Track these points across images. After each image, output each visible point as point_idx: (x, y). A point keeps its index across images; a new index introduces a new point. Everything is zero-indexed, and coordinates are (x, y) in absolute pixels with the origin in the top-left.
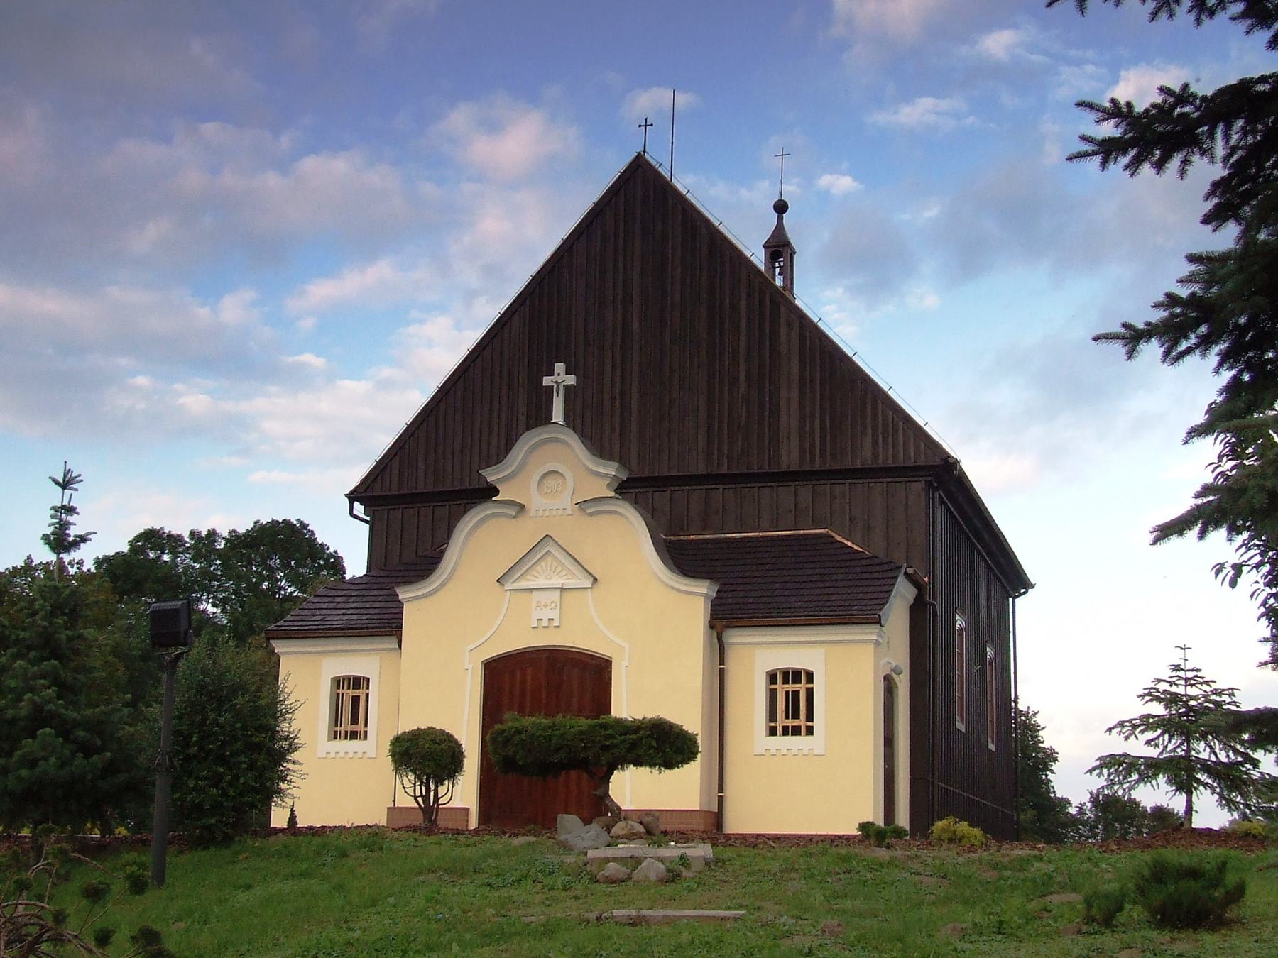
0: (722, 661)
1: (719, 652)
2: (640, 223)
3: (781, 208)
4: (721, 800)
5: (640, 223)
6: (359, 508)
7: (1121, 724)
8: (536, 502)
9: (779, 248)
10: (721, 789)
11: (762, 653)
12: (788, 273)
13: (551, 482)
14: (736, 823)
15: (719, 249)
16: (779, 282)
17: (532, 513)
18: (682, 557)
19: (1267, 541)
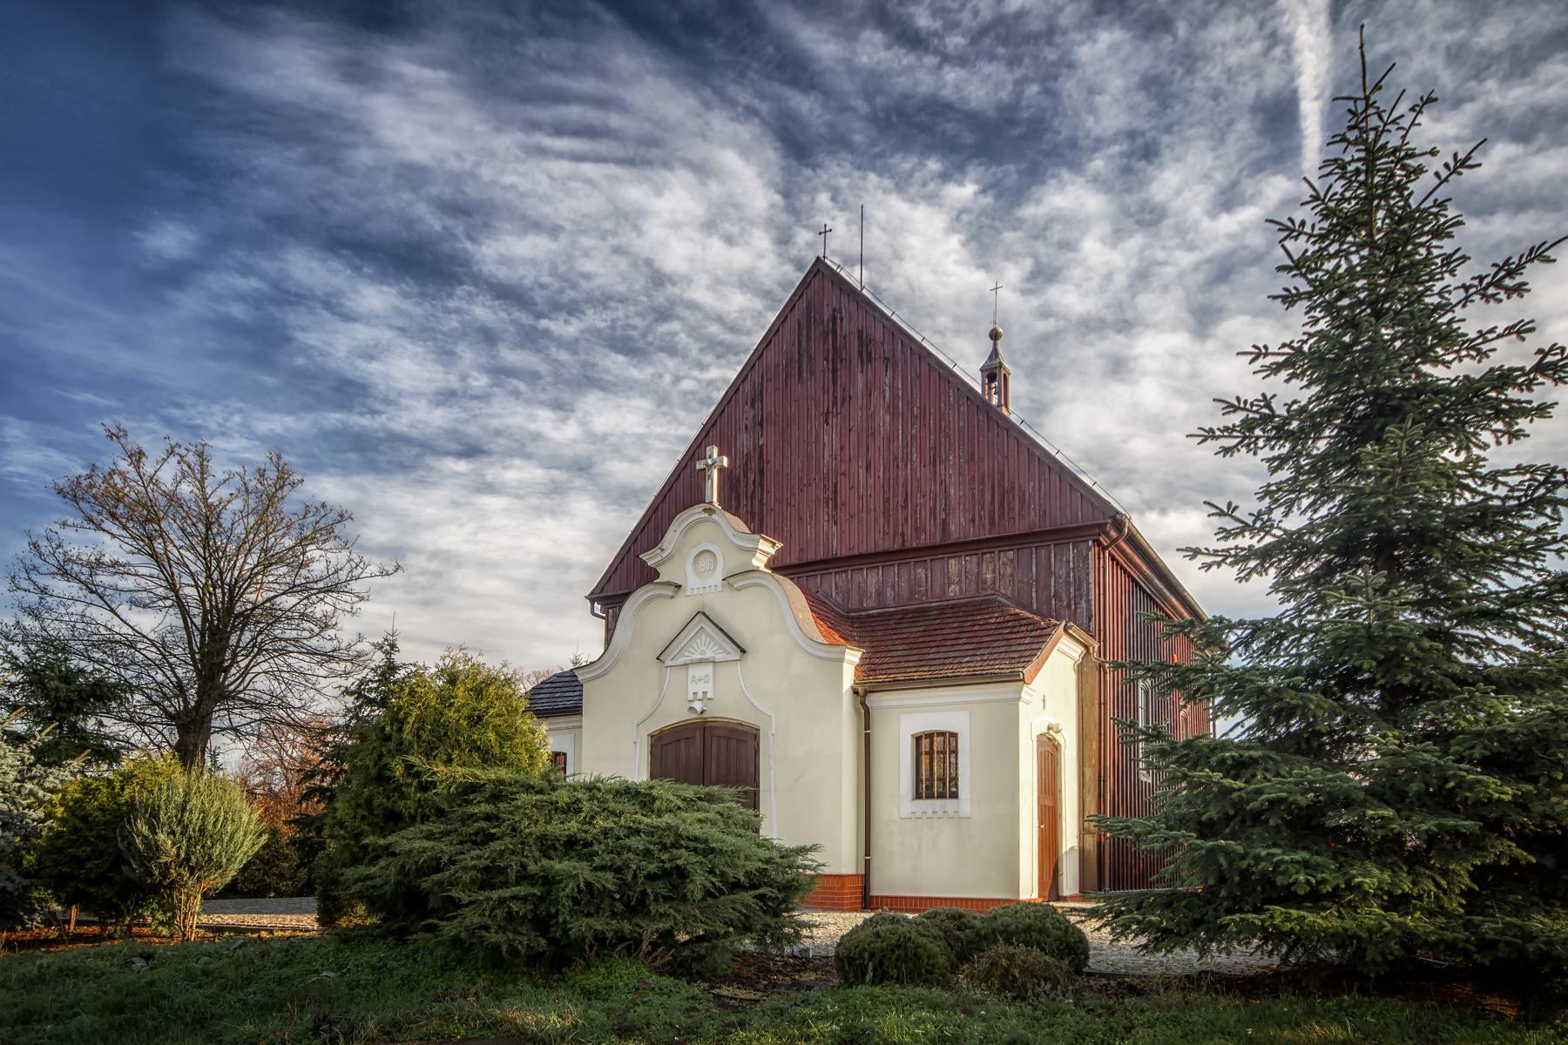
0: (867, 727)
1: (866, 718)
2: (830, 333)
3: (995, 336)
4: (868, 863)
5: (830, 333)
6: (597, 607)
7: (1188, 549)
8: (692, 582)
9: (993, 373)
10: (868, 853)
11: (911, 714)
12: (1004, 392)
13: (705, 561)
14: (877, 890)
15: (944, 376)
16: (995, 401)
17: (689, 593)
18: (844, 621)
19: (24, 910)
